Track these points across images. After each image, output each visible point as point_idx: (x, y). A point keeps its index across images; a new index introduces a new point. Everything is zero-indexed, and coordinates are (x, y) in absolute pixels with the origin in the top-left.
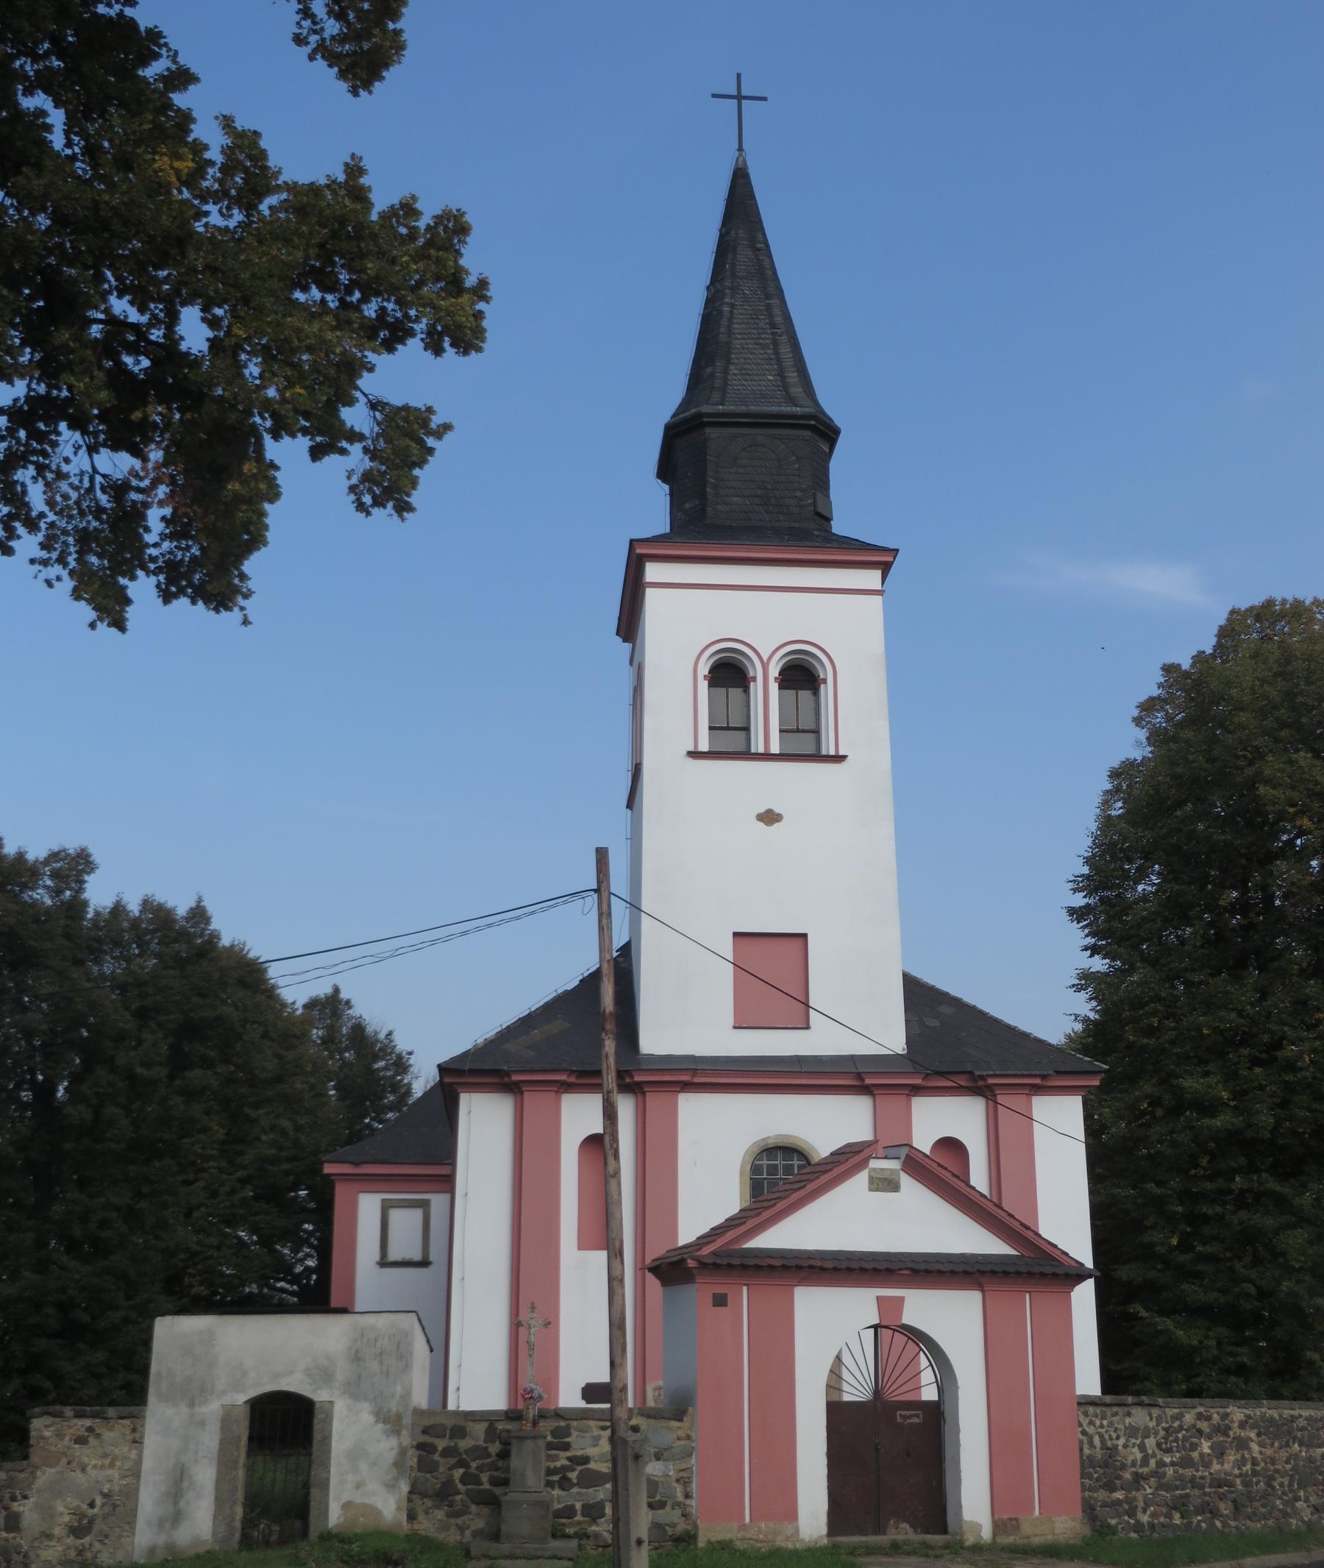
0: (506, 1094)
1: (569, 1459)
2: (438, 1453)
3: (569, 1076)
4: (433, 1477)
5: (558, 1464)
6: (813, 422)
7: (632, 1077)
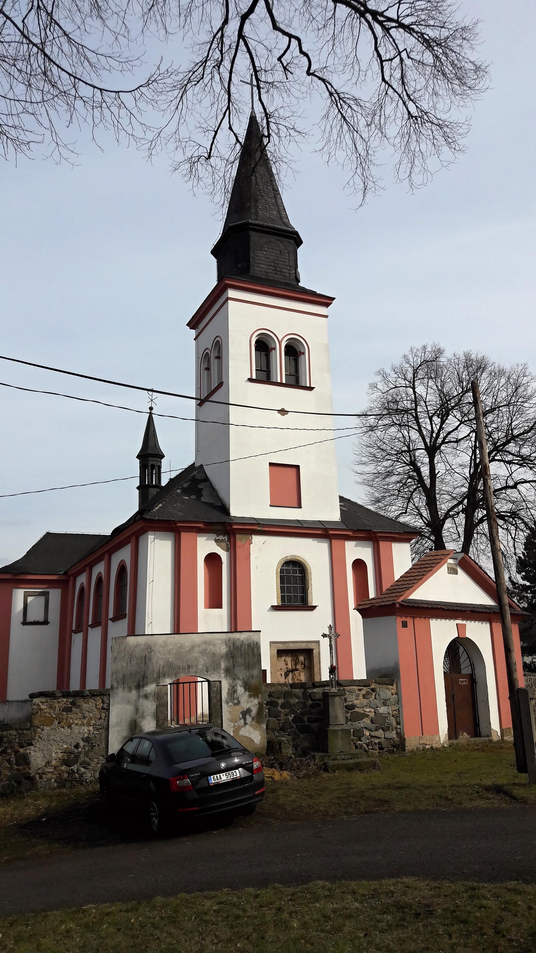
4: (277, 719)
6: (295, 236)
7: (232, 527)
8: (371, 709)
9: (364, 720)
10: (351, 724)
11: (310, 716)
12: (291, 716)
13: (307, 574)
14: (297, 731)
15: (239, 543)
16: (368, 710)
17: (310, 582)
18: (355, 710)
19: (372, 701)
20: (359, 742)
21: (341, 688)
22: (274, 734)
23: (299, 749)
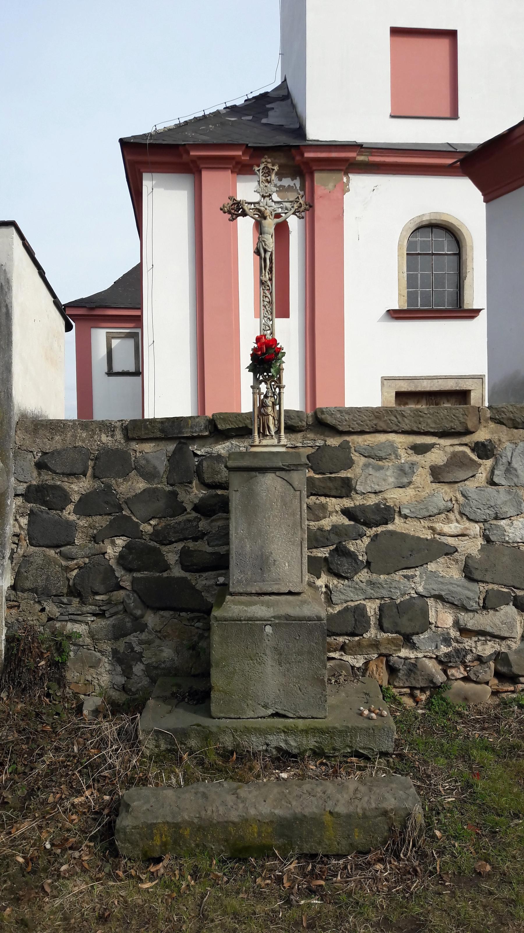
0: (189, 175)
1: (346, 512)
2: (71, 507)
3: (244, 154)
5: (326, 523)
7: (302, 155)
8: (468, 524)
9: (432, 567)
10: (371, 583)
11: (191, 545)
12: (113, 543)
13: (464, 249)
14: (132, 602)
15: (319, 190)
16: (453, 528)
17: (468, 263)
18: (390, 527)
19: (472, 495)
20: (404, 653)
21: (334, 442)
22: (43, 610)
23: (138, 669)
